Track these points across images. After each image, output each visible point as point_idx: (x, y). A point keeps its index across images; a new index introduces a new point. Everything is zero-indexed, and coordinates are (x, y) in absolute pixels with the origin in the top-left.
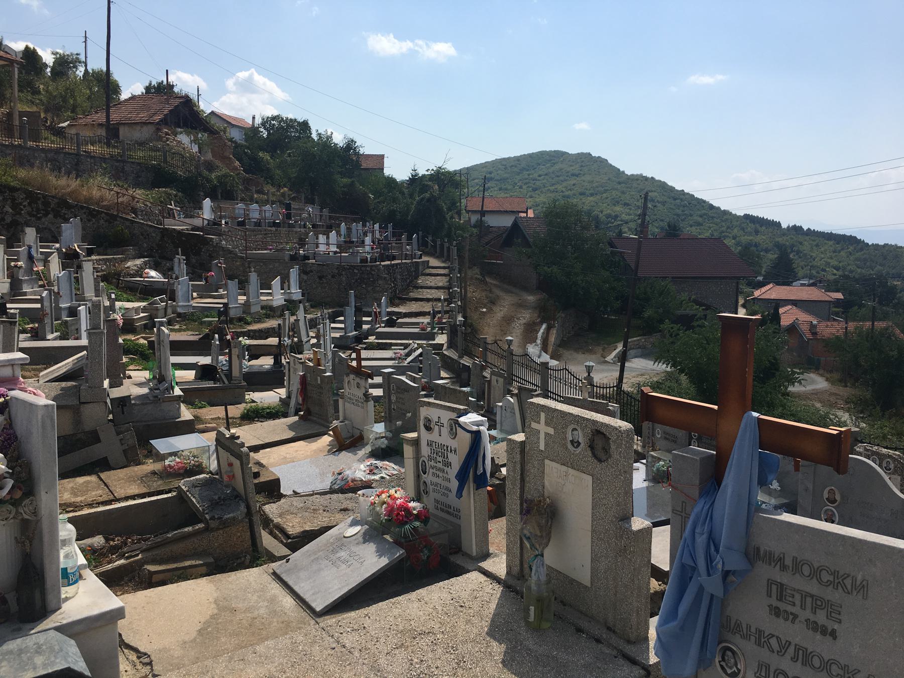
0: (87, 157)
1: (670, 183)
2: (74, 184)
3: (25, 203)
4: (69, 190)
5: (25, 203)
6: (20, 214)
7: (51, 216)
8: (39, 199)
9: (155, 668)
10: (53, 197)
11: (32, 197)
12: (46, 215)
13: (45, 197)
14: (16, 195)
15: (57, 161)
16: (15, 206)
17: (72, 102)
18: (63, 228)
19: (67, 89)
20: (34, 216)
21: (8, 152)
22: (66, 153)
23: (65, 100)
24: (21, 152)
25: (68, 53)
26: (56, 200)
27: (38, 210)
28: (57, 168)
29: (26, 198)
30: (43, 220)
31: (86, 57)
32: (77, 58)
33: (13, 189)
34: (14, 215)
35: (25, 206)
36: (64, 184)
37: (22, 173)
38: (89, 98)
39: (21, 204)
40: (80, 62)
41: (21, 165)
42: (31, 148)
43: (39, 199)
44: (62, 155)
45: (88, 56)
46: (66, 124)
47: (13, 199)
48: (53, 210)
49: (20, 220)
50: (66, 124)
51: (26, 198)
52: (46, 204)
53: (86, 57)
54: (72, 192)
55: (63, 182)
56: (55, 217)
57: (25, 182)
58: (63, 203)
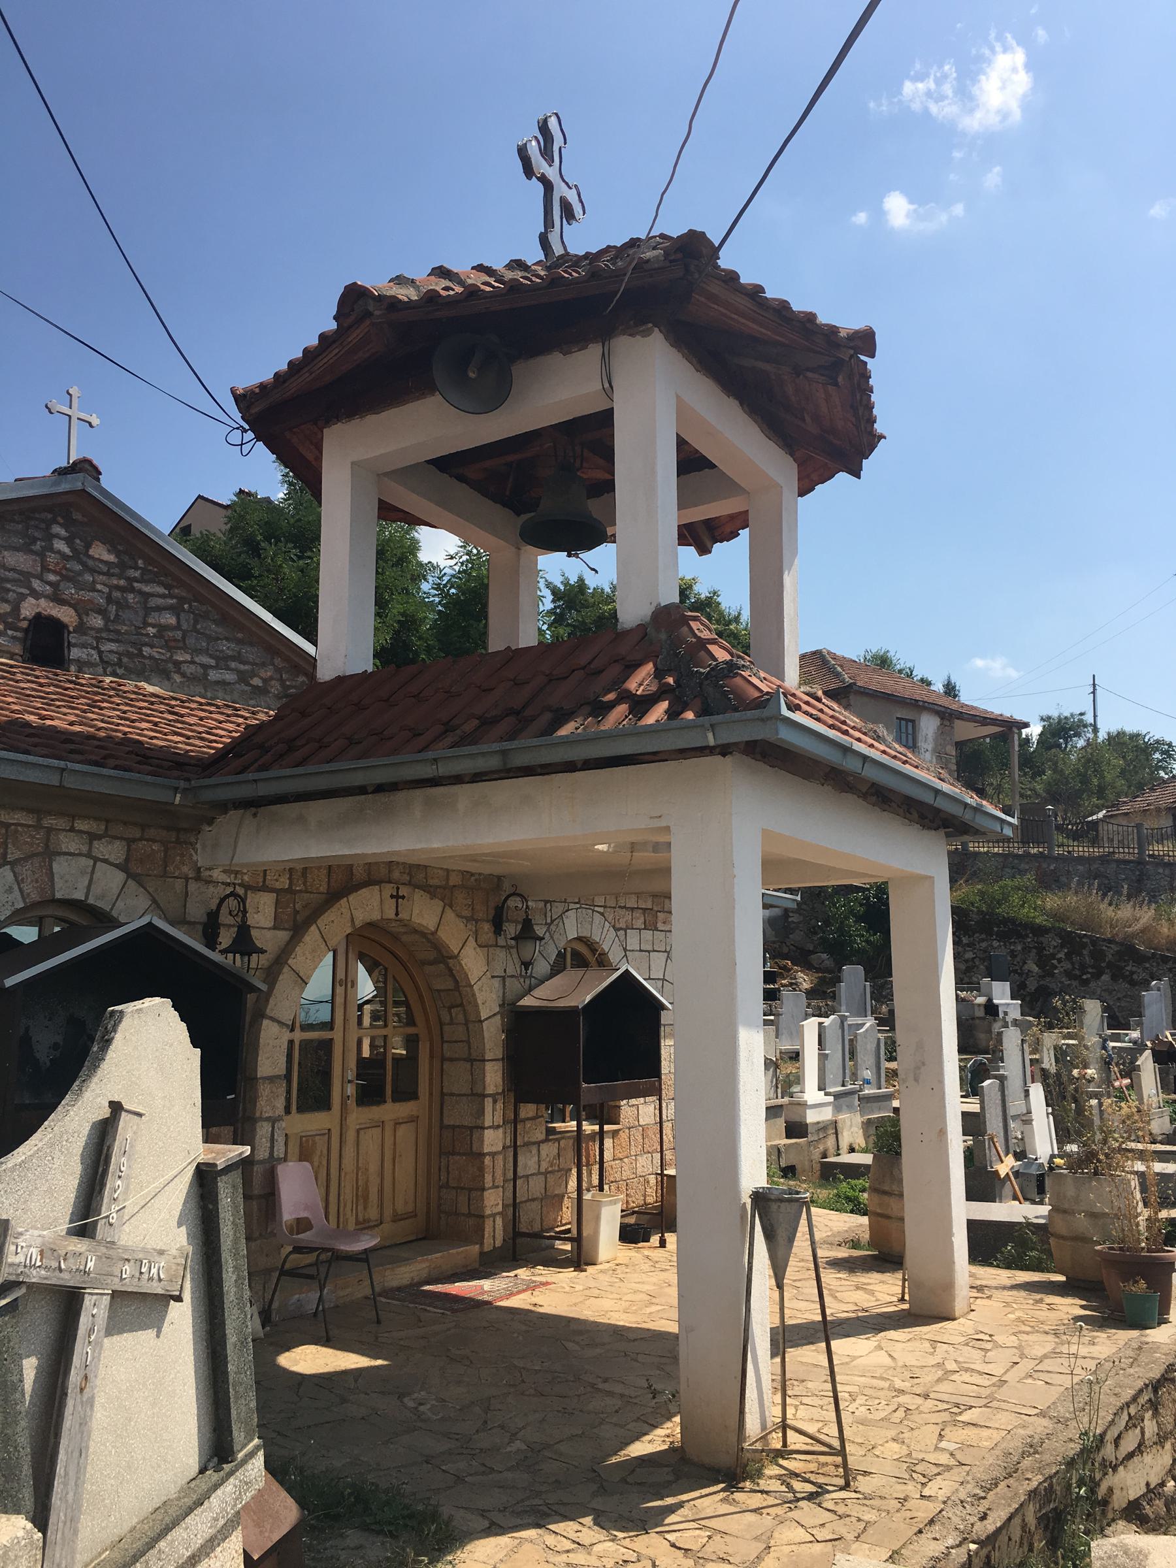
0: (1158, 865)
1: (189, 1039)
2: (1147, 915)
3: (1061, 955)
4: (1137, 927)
5: (1061, 955)
6: (1052, 975)
7: (1105, 978)
8: (1084, 946)
9: (850, 1459)
10: (1110, 941)
11: (1070, 941)
12: (1098, 975)
13: (1094, 942)
14: (1044, 940)
15: (1113, 877)
16: (1043, 962)
17: (1095, 781)
18: (1146, 1000)
19: (1089, 760)
20: (1076, 978)
21: (1023, 866)
22: (1119, 861)
23: (1085, 780)
24: (1045, 865)
25: (1067, 714)
26: (1115, 948)
27: (1083, 967)
28: (1109, 888)
29: (1062, 946)
30: (1093, 985)
31: (1095, 716)
32: (1081, 721)
33: (1040, 931)
34: (1042, 977)
35: (1060, 961)
36: (1129, 917)
37: (1052, 901)
38: (1123, 772)
39: (1053, 956)
40: (1085, 726)
41: (1048, 888)
42: (1060, 858)
43: (1084, 946)
44: (1114, 865)
45: (1099, 713)
46: (1101, 815)
47: (1040, 949)
48: (1110, 965)
49: (1053, 986)
50: (1101, 815)
51: (1062, 946)
52: (1097, 955)
53: (1095, 716)
54: (1144, 931)
55: (1126, 911)
56: (1114, 978)
57: (1056, 915)
58: (1128, 951)
